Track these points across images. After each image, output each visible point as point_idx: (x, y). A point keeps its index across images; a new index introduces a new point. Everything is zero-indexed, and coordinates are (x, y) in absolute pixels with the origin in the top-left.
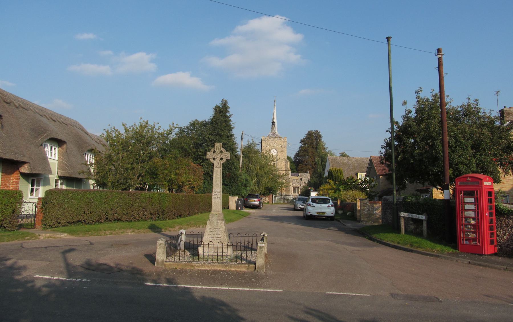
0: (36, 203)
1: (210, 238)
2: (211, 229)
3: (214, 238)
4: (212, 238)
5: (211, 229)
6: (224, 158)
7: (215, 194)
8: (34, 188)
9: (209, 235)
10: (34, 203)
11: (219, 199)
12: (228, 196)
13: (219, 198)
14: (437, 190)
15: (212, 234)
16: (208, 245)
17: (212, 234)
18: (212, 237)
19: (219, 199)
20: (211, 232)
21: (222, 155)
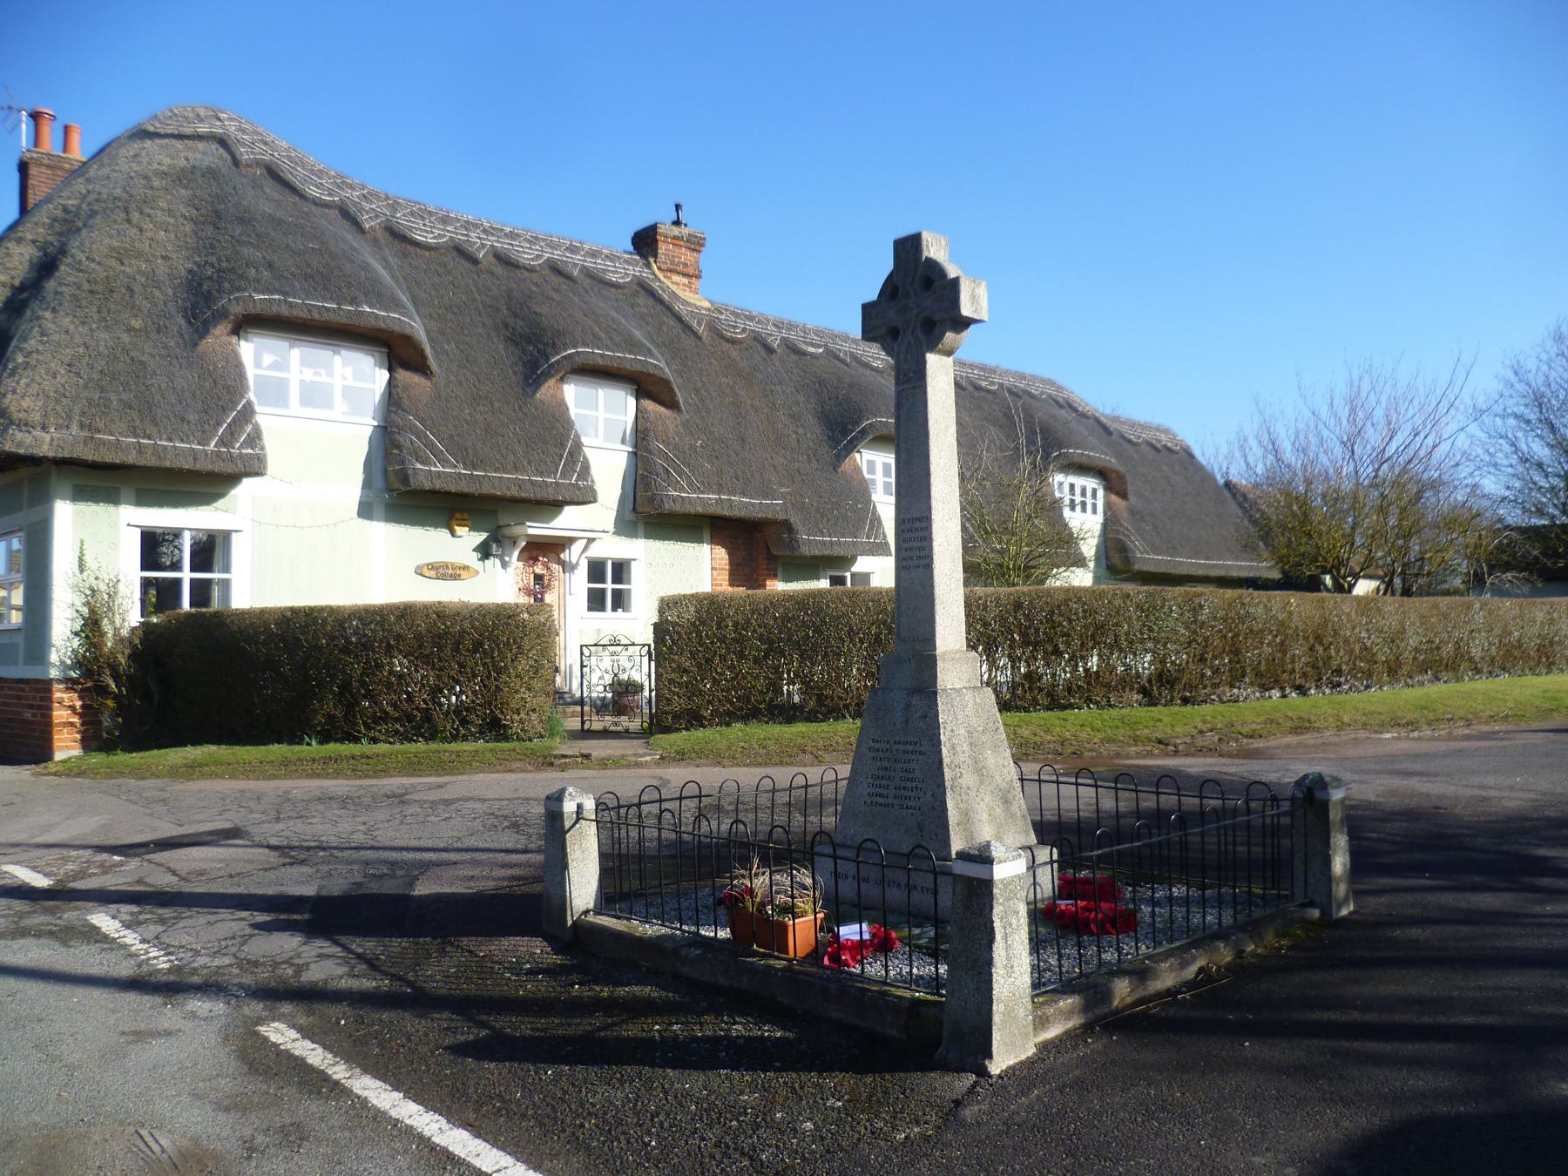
0: (649, 645)
2: (878, 746)
3: (891, 800)
4: (881, 800)
5: (878, 746)
8: (192, 570)
9: (870, 781)
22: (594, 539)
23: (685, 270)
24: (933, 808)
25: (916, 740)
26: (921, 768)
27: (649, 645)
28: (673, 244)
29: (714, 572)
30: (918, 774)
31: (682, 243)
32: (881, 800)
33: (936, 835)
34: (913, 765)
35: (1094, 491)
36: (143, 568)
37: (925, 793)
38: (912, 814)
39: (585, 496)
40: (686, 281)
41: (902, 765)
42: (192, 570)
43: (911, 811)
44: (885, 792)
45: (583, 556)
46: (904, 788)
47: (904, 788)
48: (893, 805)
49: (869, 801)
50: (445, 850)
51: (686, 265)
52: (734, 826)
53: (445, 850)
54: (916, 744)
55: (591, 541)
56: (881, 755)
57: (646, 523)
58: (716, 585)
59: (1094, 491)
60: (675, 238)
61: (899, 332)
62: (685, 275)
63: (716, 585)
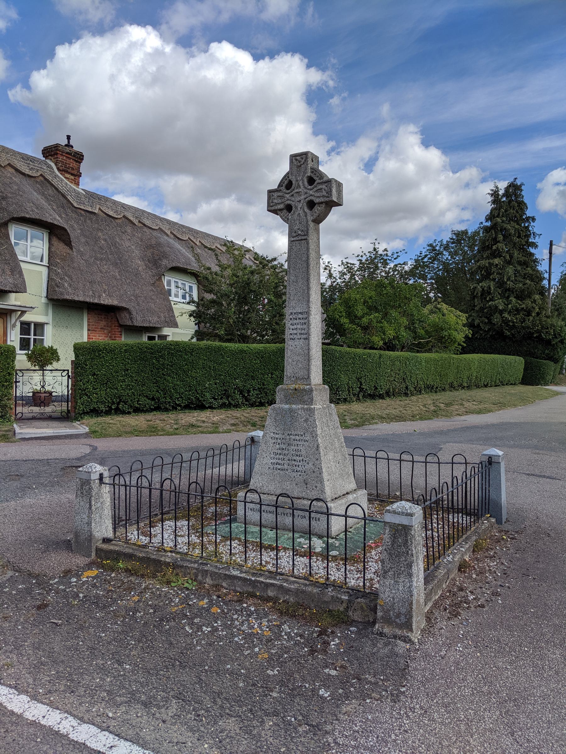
0: (68, 370)
1: (276, 466)
2: (277, 436)
3: (286, 466)
4: (279, 467)
5: (277, 436)
6: (317, 200)
7: (295, 321)
8: (29, 339)
9: (272, 456)
10: (64, 370)
11: (305, 339)
12: (558, 310)
13: (304, 336)
14: (160, 228)
15: (280, 451)
16: (453, 463)
17: (280, 451)
18: (280, 461)
19: (305, 339)
20: (278, 446)
21: (311, 192)
22: (26, 312)
23: (73, 172)
24: (314, 472)
25: (302, 433)
26: (305, 449)
27: (68, 370)
28: (66, 157)
29: (89, 332)
30: (303, 452)
31: (70, 157)
32: (279, 467)
33: (316, 487)
34: (299, 448)
35: (191, 288)
36: (43, 339)
37: (308, 463)
38: (300, 475)
39: (21, 288)
40: (73, 177)
41: (293, 447)
42: (29, 339)
43: (299, 473)
44: (282, 462)
45: (18, 321)
46: (295, 460)
47: (295, 460)
48: (287, 470)
49: (272, 467)
50: (130, 509)
51: (73, 169)
52: (140, 480)
53: (130, 509)
54: (302, 435)
55: (23, 313)
56: (279, 441)
57: (53, 305)
58: (90, 338)
59: (191, 288)
60: (67, 153)
61: (292, 207)
62: (72, 174)
63: (90, 338)
